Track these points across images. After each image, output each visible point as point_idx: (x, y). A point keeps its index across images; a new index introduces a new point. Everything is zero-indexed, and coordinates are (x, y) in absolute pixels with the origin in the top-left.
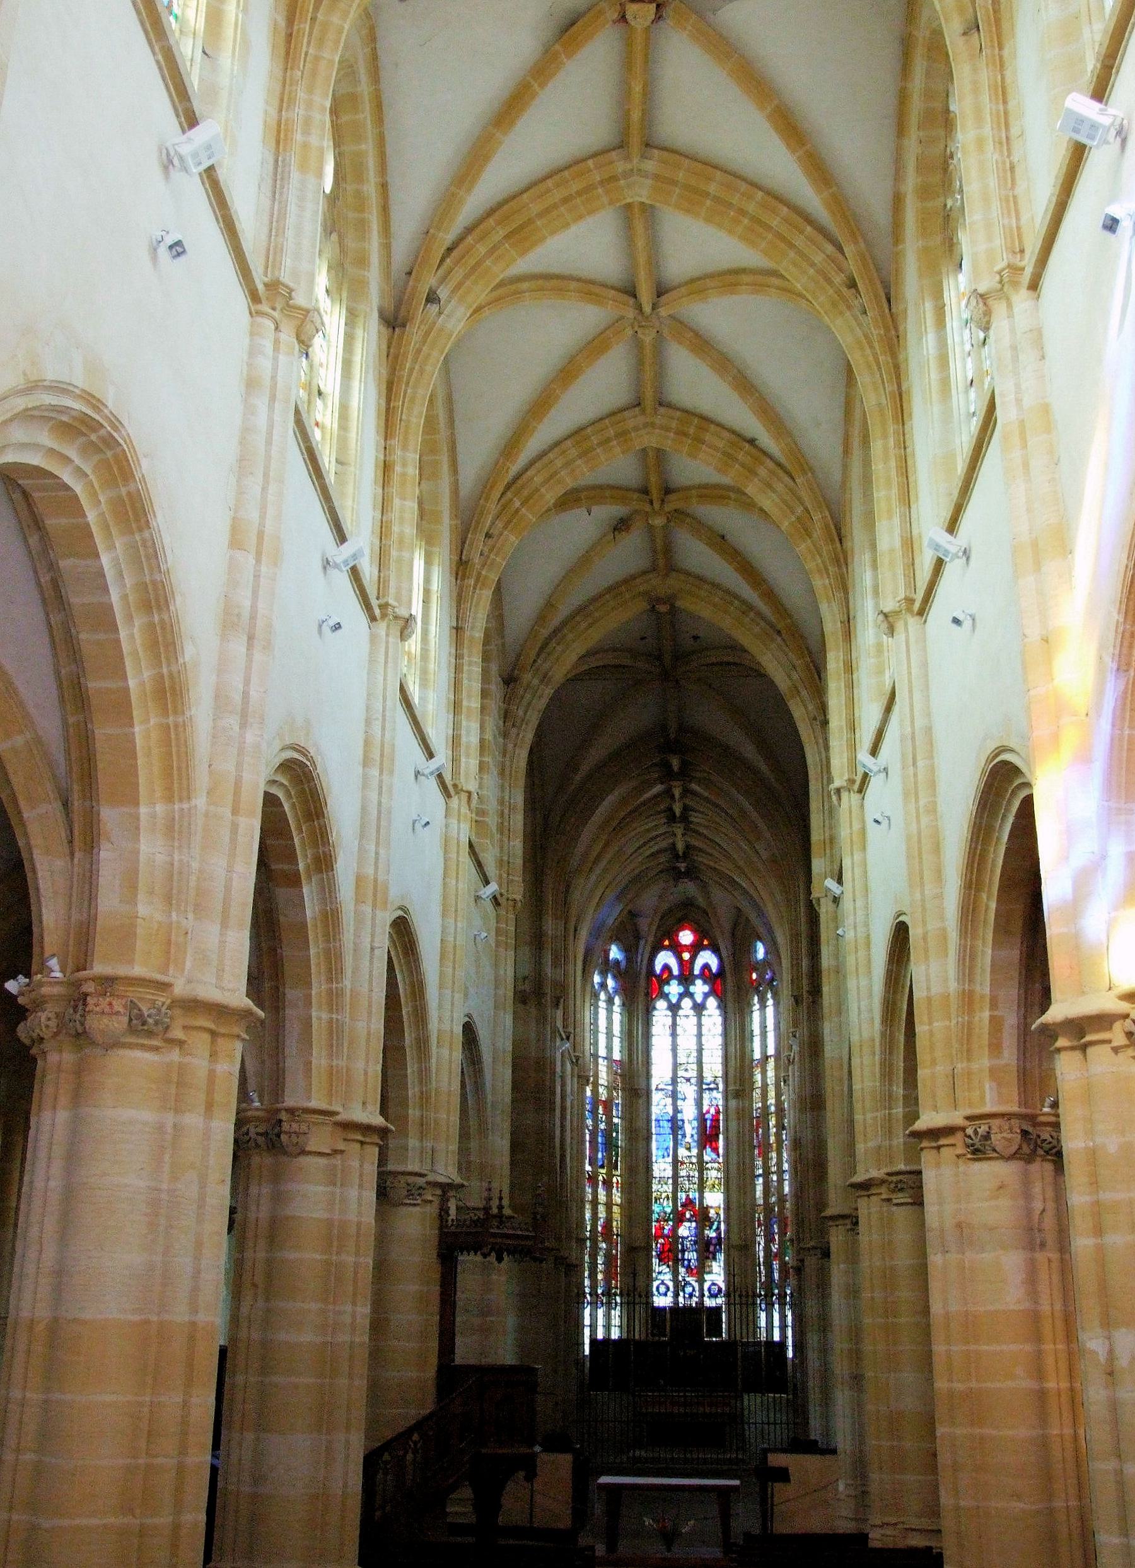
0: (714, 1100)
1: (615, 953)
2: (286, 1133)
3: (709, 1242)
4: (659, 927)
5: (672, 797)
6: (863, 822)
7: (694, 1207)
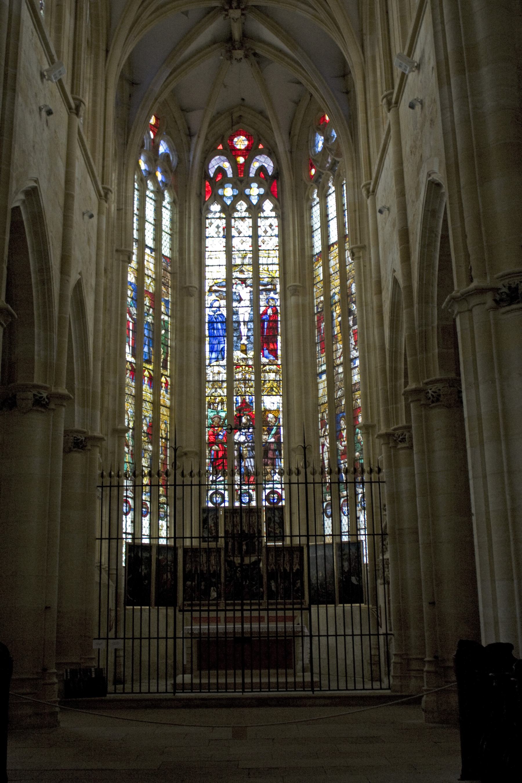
7: (251, 410)
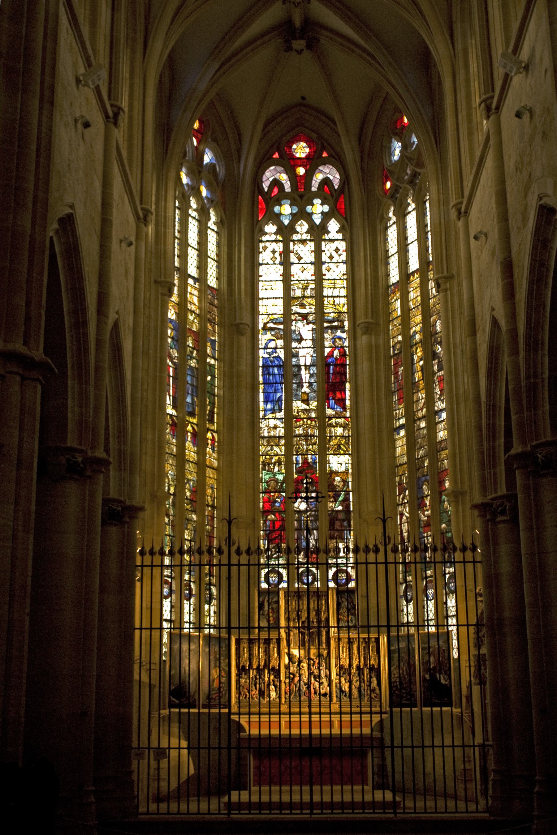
3: (333, 517)
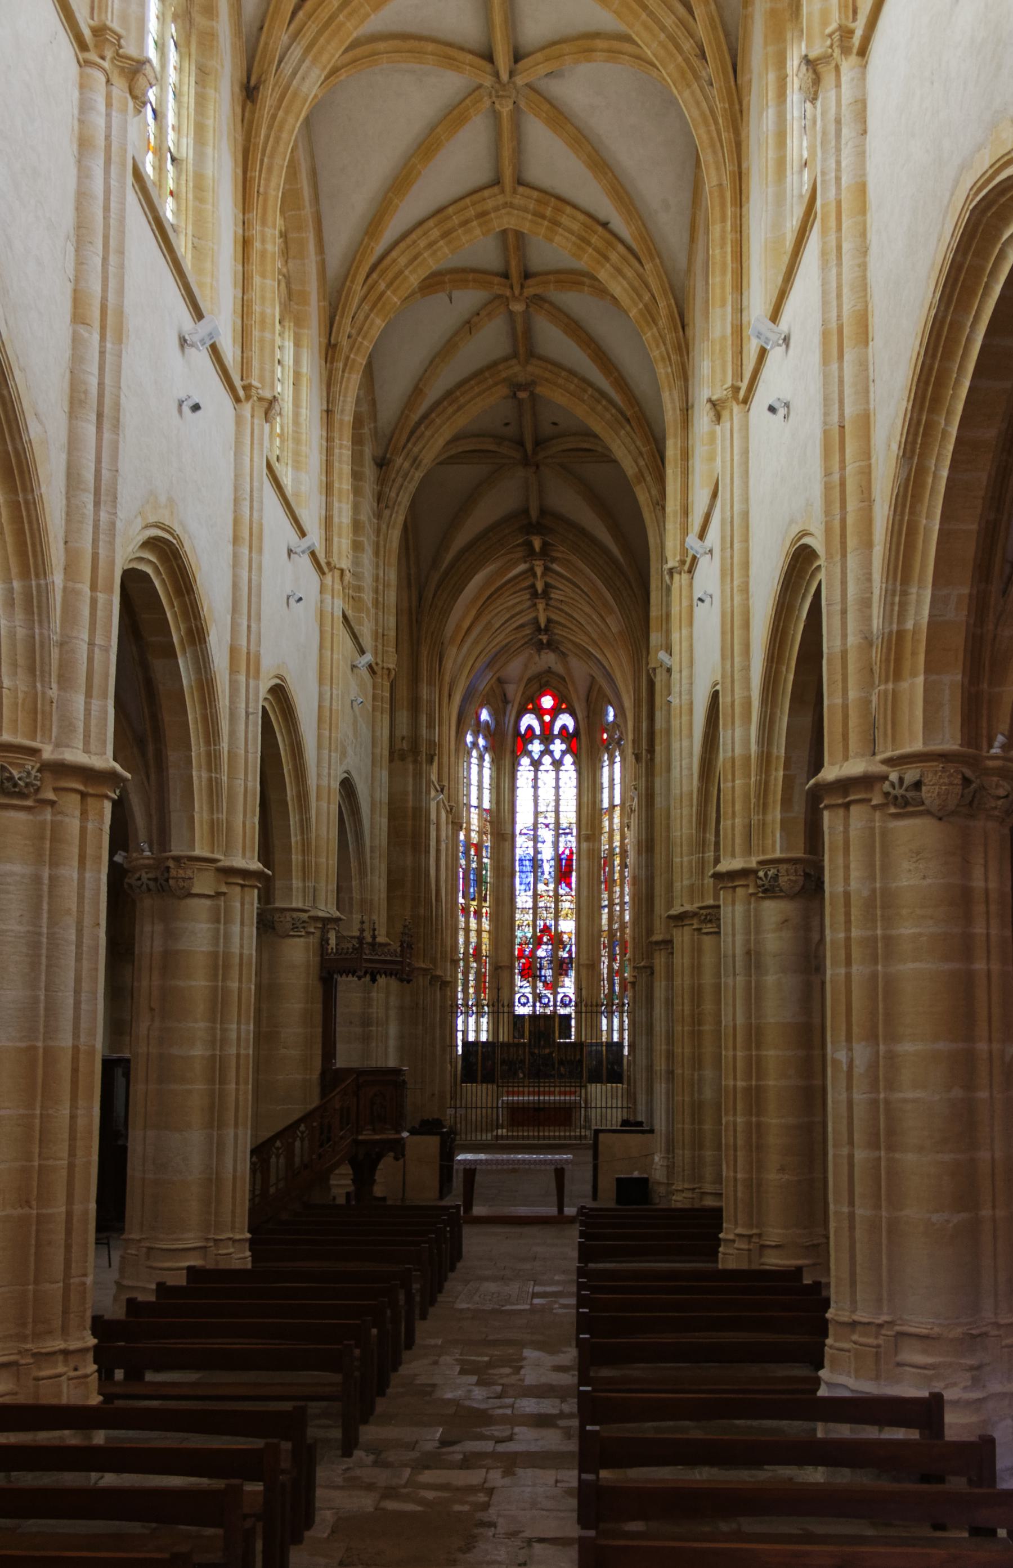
0: (569, 842)
1: (485, 715)
2: (173, 878)
4: (524, 693)
5: (534, 575)
6: (692, 599)
